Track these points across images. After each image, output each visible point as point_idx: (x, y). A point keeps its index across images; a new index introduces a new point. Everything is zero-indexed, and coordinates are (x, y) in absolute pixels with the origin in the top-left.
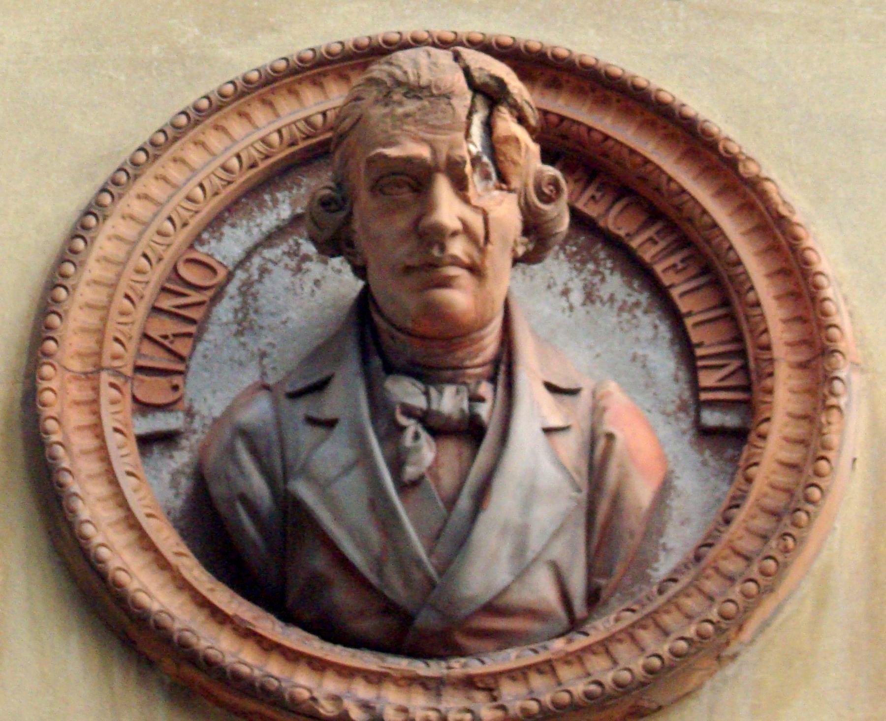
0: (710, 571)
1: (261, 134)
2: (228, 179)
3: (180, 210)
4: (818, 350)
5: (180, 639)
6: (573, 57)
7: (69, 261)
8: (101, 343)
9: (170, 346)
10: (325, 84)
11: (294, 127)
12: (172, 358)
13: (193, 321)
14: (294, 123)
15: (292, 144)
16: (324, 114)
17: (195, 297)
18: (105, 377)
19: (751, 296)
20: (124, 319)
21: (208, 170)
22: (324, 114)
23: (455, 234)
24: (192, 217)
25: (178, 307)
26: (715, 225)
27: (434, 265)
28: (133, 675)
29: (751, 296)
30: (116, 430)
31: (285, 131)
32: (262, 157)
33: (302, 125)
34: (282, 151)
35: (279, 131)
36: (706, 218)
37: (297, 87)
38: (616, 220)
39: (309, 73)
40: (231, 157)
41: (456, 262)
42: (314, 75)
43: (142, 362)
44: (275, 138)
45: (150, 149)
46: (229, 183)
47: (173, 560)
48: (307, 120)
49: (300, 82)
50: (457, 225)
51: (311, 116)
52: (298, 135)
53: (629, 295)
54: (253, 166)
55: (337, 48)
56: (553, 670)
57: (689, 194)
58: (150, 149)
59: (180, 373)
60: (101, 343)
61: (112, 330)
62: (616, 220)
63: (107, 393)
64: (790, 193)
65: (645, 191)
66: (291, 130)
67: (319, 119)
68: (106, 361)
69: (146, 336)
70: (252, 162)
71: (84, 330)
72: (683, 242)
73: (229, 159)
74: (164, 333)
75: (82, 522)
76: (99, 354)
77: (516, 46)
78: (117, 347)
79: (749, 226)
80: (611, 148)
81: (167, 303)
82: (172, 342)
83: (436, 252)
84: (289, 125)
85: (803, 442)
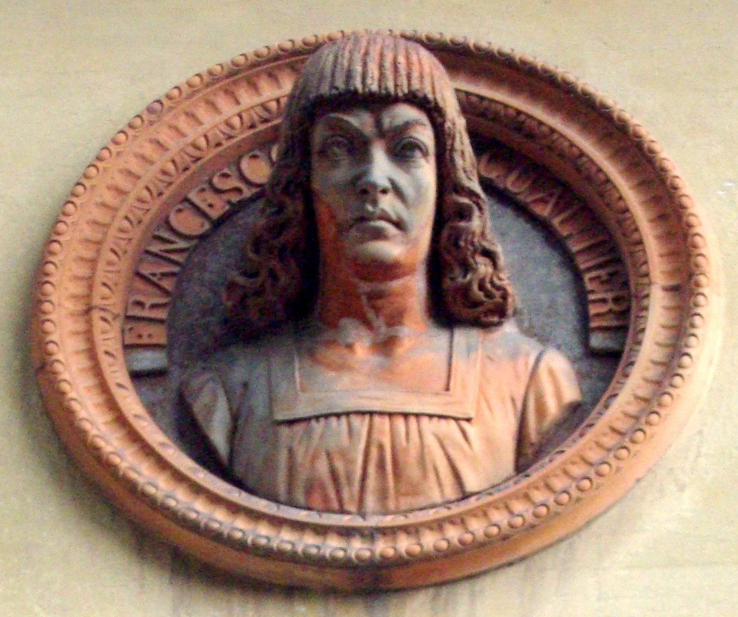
1: (224, 117)
7: (55, 241)
8: (91, 287)
9: (157, 282)
10: (280, 77)
12: (158, 292)
13: (176, 263)
14: (252, 108)
16: (278, 101)
17: (182, 244)
18: (96, 315)
19: (636, 236)
20: (110, 268)
22: (278, 101)
23: (384, 192)
25: (167, 251)
26: (608, 180)
27: (363, 219)
28: (290, 529)
29: (636, 236)
31: (244, 115)
32: (165, 184)
33: (259, 110)
34: (242, 132)
35: (240, 116)
36: (601, 176)
37: (276, 72)
38: (510, 183)
41: (385, 217)
42: (272, 68)
44: (236, 121)
46: (170, 184)
48: (264, 106)
49: (279, 68)
50: (387, 184)
52: (256, 118)
55: (288, 45)
56: (463, 521)
57: (588, 156)
58: (164, 101)
60: (91, 287)
61: (100, 277)
62: (510, 183)
63: (99, 325)
67: (273, 105)
68: (97, 301)
69: (139, 275)
71: (76, 278)
73: (122, 201)
75: (81, 419)
76: (89, 296)
77: (443, 39)
78: (106, 291)
80: (523, 123)
81: (156, 248)
83: (370, 208)
84: (248, 110)
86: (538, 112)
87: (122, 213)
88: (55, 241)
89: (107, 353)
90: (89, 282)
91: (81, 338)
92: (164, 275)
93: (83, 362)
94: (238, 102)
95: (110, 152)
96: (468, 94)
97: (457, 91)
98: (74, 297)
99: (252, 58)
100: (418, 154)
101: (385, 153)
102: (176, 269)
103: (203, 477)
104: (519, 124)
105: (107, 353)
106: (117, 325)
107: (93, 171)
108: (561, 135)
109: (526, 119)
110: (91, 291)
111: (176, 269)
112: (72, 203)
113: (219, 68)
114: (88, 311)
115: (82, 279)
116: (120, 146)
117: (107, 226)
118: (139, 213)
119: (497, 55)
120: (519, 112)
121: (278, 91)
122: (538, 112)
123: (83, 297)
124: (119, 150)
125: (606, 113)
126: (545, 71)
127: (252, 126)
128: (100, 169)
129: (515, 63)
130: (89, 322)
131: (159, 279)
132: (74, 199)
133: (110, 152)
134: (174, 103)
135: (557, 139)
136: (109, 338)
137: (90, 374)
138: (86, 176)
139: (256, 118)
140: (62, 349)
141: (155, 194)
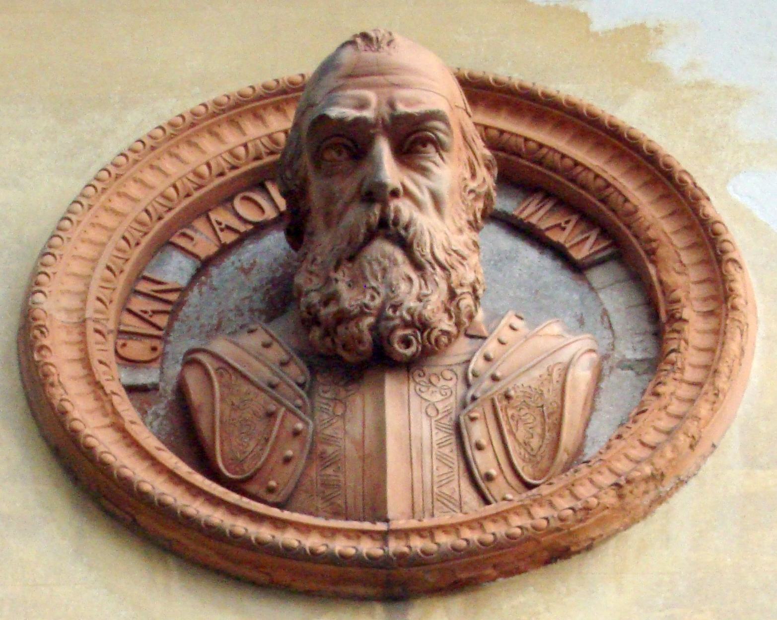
0: (622, 457)
2: (199, 183)
3: (157, 205)
4: (722, 297)
5: (159, 501)
6: (513, 80)
7: (49, 254)
11: (220, 159)
15: (258, 158)
20: (120, 255)
21: (147, 201)
24: (142, 237)
25: (157, 291)
30: (97, 331)
31: (250, 145)
32: (166, 209)
33: (265, 141)
34: (247, 163)
35: (245, 146)
36: (628, 205)
37: (261, 112)
39: (206, 123)
40: (140, 213)
43: (122, 328)
45: (169, 130)
47: (155, 453)
51: (273, 133)
53: (666, 398)
54: (222, 174)
59: (132, 227)
60: (84, 301)
64: (633, 114)
65: (591, 197)
66: (256, 145)
70: (220, 171)
72: (588, 218)
74: (144, 309)
76: (83, 309)
79: (641, 182)
82: (151, 316)
85: (707, 367)
86: (580, 153)
87: (143, 205)
88: (49, 254)
89: (101, 362)
90: (83, 296)
91: (76, 348)
92: (155, 312)
93: (78, 369)
94: (244, 134)
95: (110, 173)
96: (486, 128)
97: (476, 124)
98: (68, 311)
99: (259, 91)
100: (430, 148)
101: (374, 148)
102: (169, 308)
103: (199, 480)
104: (538, 155)
105: (101, 362)
106: (111, 338)
107: (67, 223)
108: (551, 149)
109: (547, 153)
110: (85, 304)
111: (169, 308)
112: (69, 219)
113: (226, 99)
114: (83, 322)
115: (78, 294)
116: (68, 232)
117: (103, 245)
118: (138, 235)
119: (567, 106)
120: (541, 146)
121: (279, 124)
122: (580, 153)
123: (76, 310)
124: (118, 172)
125: (634, 144)
126: (569, 103)
127: (258, 158)
128: (98, 188)
129: (516, 90)
130: (83, 334)
131: (222, 230)
132: (60, 233)
133: (110, 173)
134: (176, 130)
135: (580, 173)
136: (102, 350)
137: (85, 381)
138: (59, 229)
139: (263, 149)
140: (53, 354)
141: (155, 217)
